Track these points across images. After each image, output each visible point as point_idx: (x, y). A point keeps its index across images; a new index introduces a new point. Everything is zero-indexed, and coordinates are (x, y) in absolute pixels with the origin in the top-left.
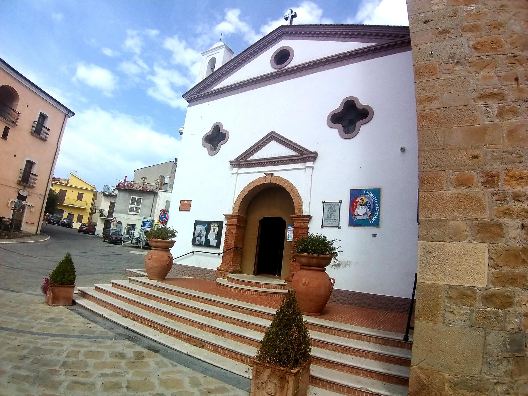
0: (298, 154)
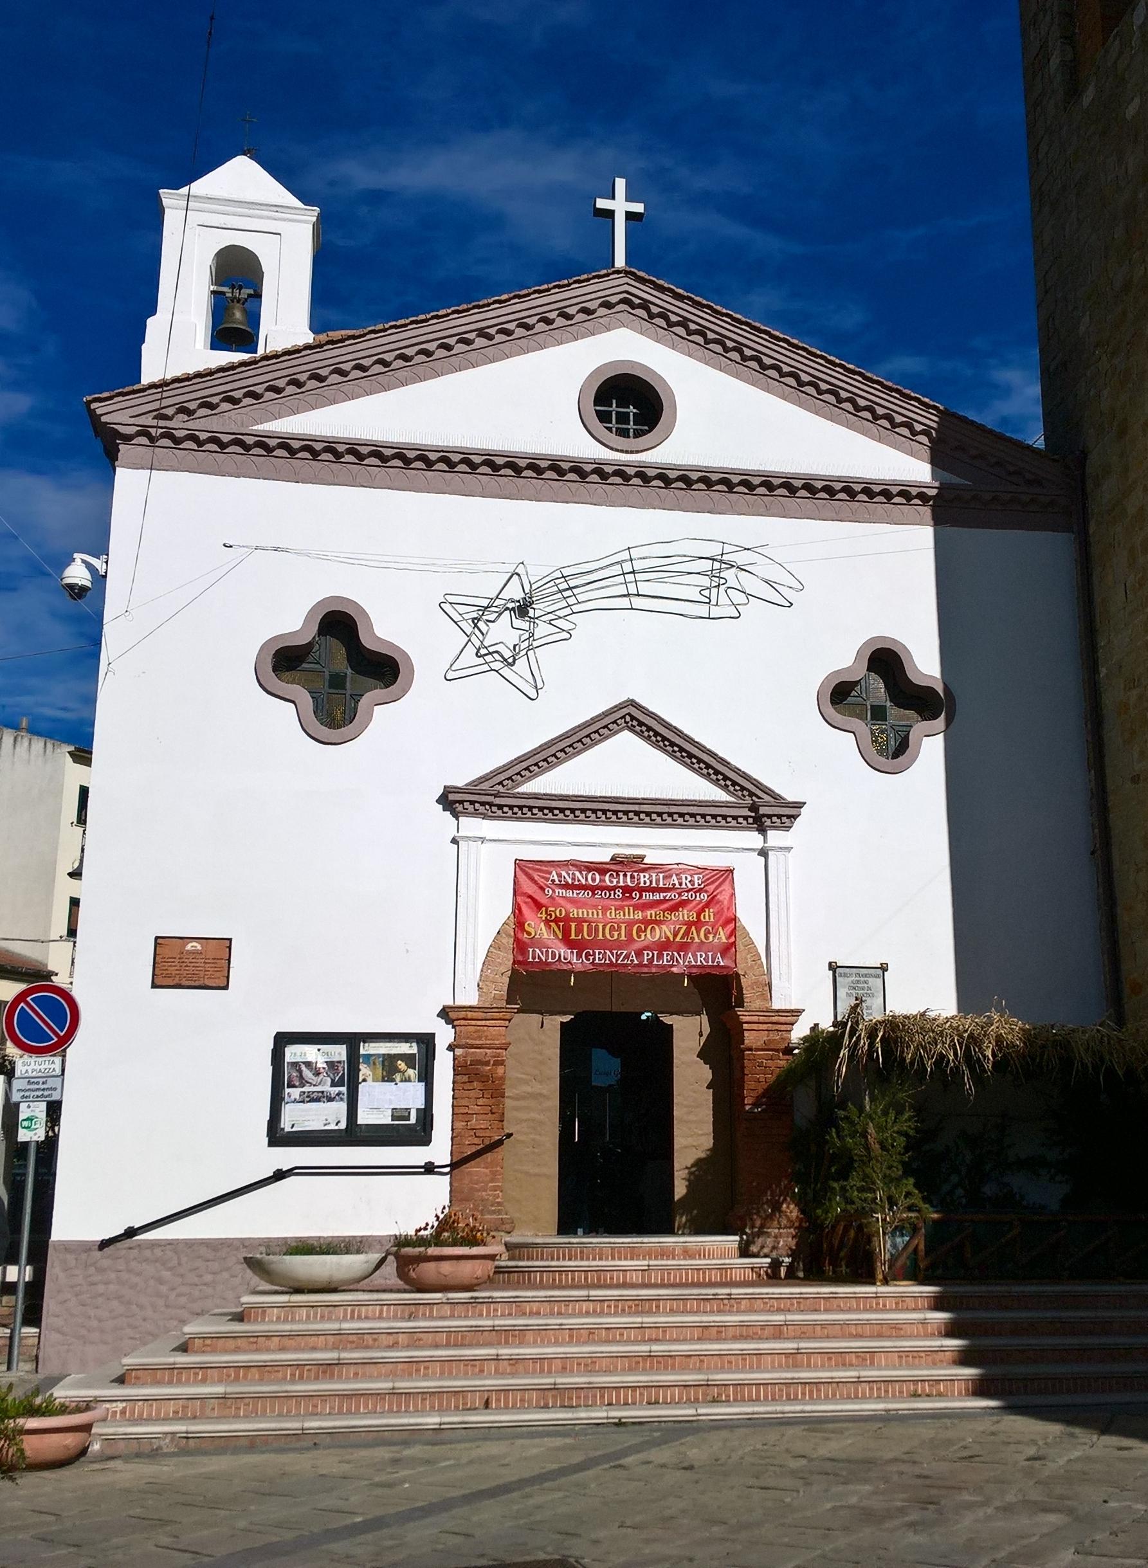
0: (733, 800)
